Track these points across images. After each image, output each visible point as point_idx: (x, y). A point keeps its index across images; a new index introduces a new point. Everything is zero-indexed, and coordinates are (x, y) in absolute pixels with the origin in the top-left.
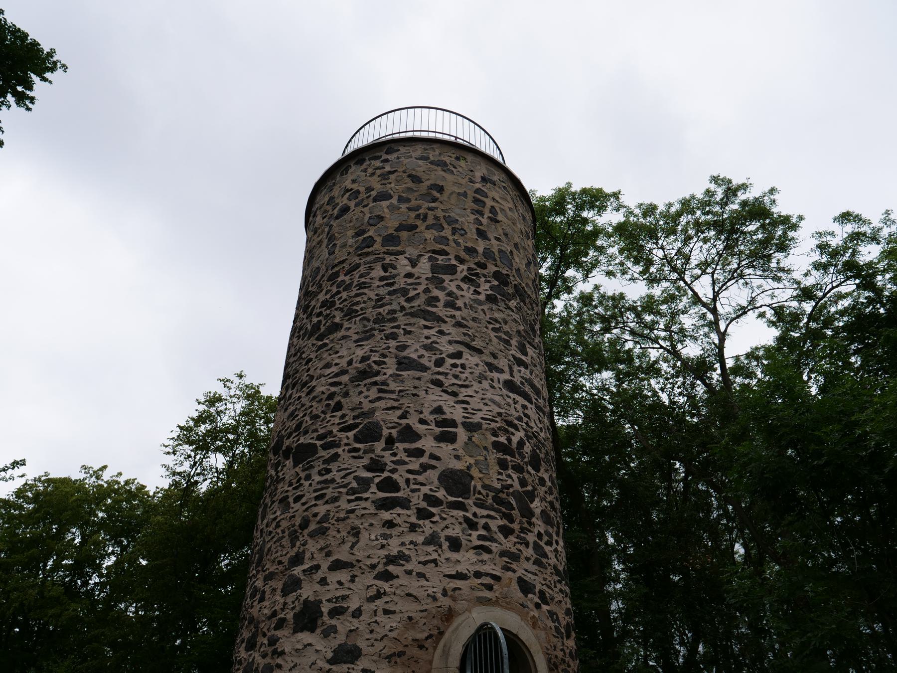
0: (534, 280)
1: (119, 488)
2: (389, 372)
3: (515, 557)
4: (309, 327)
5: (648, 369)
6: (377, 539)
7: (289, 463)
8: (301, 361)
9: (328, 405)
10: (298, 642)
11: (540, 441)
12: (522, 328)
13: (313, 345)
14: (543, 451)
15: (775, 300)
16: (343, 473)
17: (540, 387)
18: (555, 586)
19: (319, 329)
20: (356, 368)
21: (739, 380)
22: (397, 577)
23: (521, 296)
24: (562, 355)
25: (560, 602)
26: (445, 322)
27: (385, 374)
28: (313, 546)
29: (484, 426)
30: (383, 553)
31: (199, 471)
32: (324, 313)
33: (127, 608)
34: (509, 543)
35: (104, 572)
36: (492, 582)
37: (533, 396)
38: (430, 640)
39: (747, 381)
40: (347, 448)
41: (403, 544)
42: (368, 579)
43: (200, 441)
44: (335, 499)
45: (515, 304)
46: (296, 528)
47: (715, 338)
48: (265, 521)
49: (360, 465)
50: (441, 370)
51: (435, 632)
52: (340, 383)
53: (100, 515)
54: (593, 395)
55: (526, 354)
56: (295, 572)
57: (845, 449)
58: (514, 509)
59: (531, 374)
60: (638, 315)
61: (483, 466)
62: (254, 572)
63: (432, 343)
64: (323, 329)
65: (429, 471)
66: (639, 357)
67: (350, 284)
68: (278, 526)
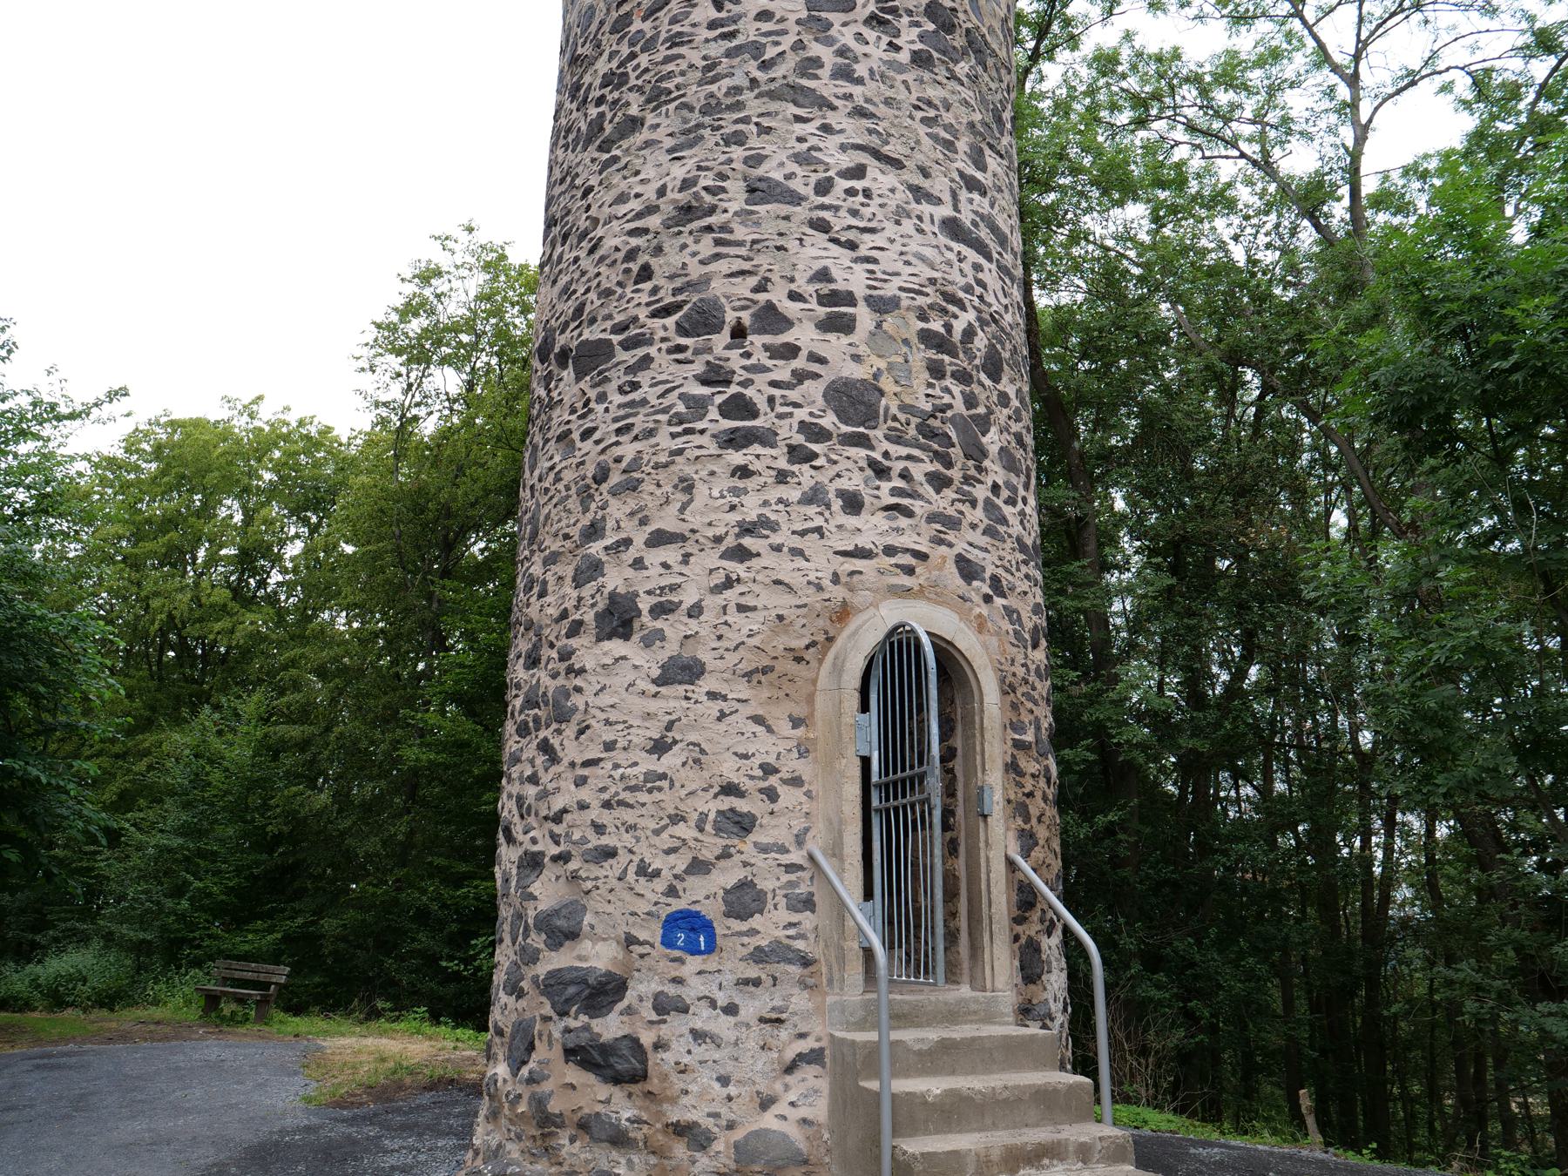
0: (1005, 20)
1: (290, 433)
2: (734, 207)
3: (953, 523)
4: (584, 128)
5: (1213, 198)
6: (723, 497)
7: (568, 374)
8: (574, 192)
9: (627, 271)
10: (605, 654)
11: (1002, 329)
12: (977, 117)
13: (593, 160)
14: (1008, 346)
15: (1479, 56)
16: (661, 389)
17: (1007, 231)
18: (1018, 570)
19: (602, 129)
20: (674, 201)
21: (1382, 217)
22: (758, 555)
23: (978, 52)
24: (1053, 173)
25: (1025, 593)
26: (834, 108)
27: (726, 211)
28: (617, 510)
29: (905, 303)
30: (734, 517)
31: (418, 398)
32: (609, 98)
33: (333, 619)
34: (943, 501)
35: (289, 565)
36: (913, 561)
37: (994, 247)
38: (812, 650)
39: (1396, 220)
40: (664, 346)
41: (766, 503)
42: (712, 558)
43: (413, 347)
44: (650, 433)
45: (966, 69)
46: (589, 481)
47: (1347, 135)
48: (536, 473)
49: (689, 375)
50: (826, 200)
51: (821, 638)
52: (646, 231)
53: (267, 476)
54: (1108, 249)
55: (983, 168)
56: (592, 551)
57: (1555, 341)
58: (953, 445)
59: (992, 206)
60: (1204, 92)
61: (901, 373)
62: (527, 553)
63: (810, 149)
64: (608, 128)
65: (807, 383)
66: (1198, 176)
67: (654, 39)
68: (558, 479)
